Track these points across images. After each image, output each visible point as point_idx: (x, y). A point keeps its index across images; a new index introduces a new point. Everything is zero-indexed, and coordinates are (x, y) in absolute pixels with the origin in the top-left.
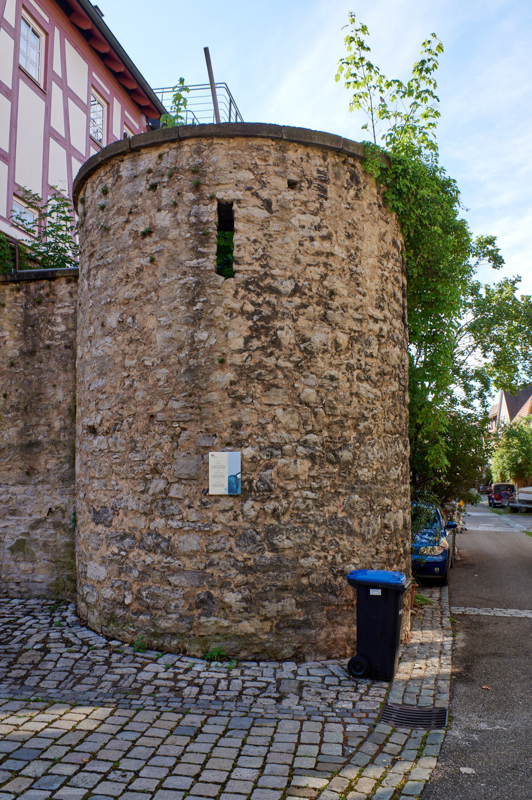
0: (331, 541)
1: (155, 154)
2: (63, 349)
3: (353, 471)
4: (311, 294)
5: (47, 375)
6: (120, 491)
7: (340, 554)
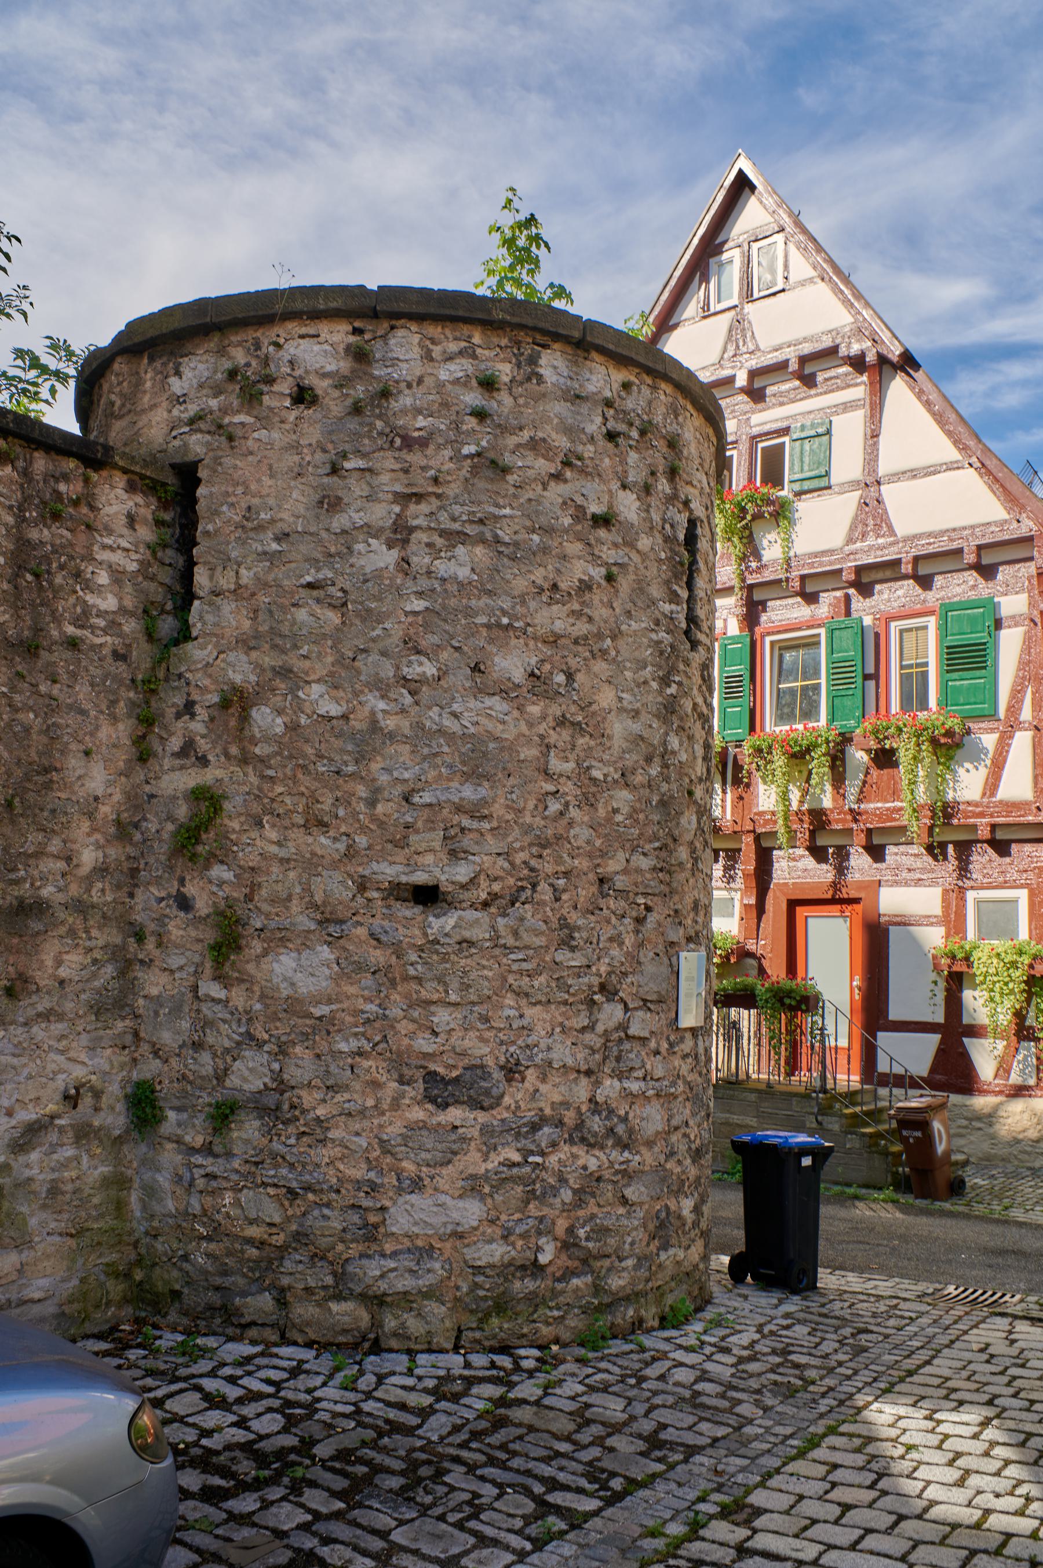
1: (619, 376)
2: (110, 660)
5: (70, 720)
6: (529, 1029)
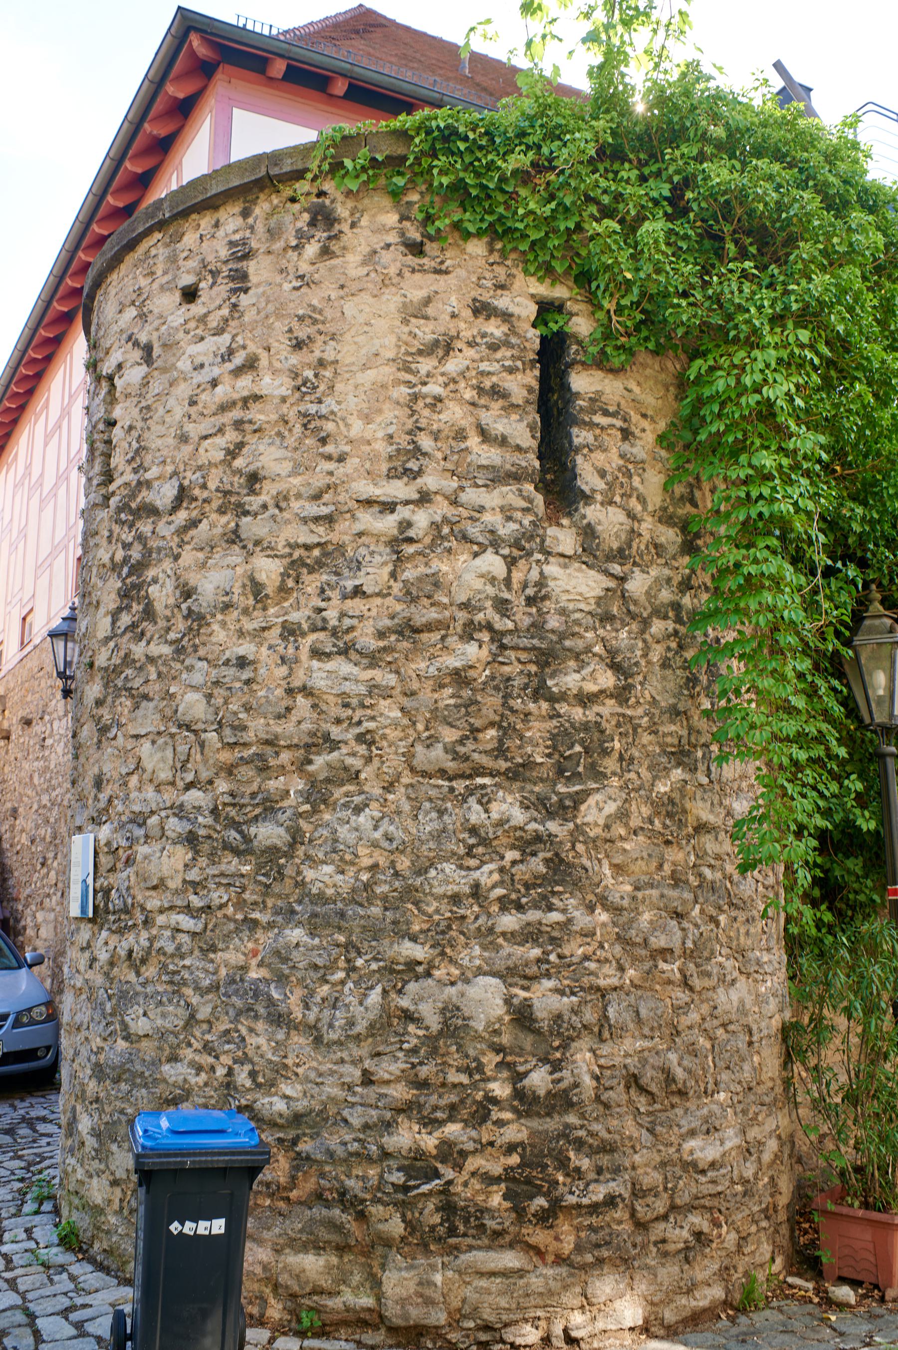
0: (227, 1032)
3: (289, 871)
4: (206, 494)
7: (247, 1067)
